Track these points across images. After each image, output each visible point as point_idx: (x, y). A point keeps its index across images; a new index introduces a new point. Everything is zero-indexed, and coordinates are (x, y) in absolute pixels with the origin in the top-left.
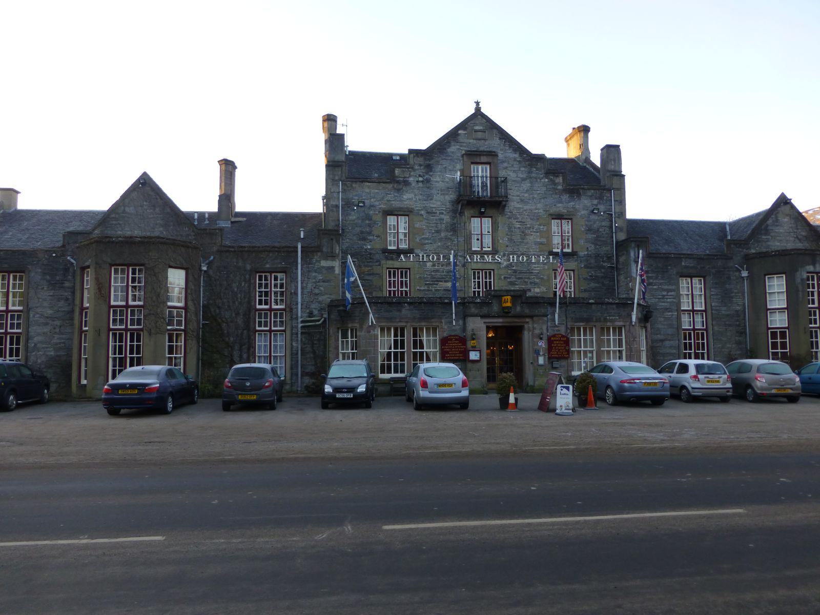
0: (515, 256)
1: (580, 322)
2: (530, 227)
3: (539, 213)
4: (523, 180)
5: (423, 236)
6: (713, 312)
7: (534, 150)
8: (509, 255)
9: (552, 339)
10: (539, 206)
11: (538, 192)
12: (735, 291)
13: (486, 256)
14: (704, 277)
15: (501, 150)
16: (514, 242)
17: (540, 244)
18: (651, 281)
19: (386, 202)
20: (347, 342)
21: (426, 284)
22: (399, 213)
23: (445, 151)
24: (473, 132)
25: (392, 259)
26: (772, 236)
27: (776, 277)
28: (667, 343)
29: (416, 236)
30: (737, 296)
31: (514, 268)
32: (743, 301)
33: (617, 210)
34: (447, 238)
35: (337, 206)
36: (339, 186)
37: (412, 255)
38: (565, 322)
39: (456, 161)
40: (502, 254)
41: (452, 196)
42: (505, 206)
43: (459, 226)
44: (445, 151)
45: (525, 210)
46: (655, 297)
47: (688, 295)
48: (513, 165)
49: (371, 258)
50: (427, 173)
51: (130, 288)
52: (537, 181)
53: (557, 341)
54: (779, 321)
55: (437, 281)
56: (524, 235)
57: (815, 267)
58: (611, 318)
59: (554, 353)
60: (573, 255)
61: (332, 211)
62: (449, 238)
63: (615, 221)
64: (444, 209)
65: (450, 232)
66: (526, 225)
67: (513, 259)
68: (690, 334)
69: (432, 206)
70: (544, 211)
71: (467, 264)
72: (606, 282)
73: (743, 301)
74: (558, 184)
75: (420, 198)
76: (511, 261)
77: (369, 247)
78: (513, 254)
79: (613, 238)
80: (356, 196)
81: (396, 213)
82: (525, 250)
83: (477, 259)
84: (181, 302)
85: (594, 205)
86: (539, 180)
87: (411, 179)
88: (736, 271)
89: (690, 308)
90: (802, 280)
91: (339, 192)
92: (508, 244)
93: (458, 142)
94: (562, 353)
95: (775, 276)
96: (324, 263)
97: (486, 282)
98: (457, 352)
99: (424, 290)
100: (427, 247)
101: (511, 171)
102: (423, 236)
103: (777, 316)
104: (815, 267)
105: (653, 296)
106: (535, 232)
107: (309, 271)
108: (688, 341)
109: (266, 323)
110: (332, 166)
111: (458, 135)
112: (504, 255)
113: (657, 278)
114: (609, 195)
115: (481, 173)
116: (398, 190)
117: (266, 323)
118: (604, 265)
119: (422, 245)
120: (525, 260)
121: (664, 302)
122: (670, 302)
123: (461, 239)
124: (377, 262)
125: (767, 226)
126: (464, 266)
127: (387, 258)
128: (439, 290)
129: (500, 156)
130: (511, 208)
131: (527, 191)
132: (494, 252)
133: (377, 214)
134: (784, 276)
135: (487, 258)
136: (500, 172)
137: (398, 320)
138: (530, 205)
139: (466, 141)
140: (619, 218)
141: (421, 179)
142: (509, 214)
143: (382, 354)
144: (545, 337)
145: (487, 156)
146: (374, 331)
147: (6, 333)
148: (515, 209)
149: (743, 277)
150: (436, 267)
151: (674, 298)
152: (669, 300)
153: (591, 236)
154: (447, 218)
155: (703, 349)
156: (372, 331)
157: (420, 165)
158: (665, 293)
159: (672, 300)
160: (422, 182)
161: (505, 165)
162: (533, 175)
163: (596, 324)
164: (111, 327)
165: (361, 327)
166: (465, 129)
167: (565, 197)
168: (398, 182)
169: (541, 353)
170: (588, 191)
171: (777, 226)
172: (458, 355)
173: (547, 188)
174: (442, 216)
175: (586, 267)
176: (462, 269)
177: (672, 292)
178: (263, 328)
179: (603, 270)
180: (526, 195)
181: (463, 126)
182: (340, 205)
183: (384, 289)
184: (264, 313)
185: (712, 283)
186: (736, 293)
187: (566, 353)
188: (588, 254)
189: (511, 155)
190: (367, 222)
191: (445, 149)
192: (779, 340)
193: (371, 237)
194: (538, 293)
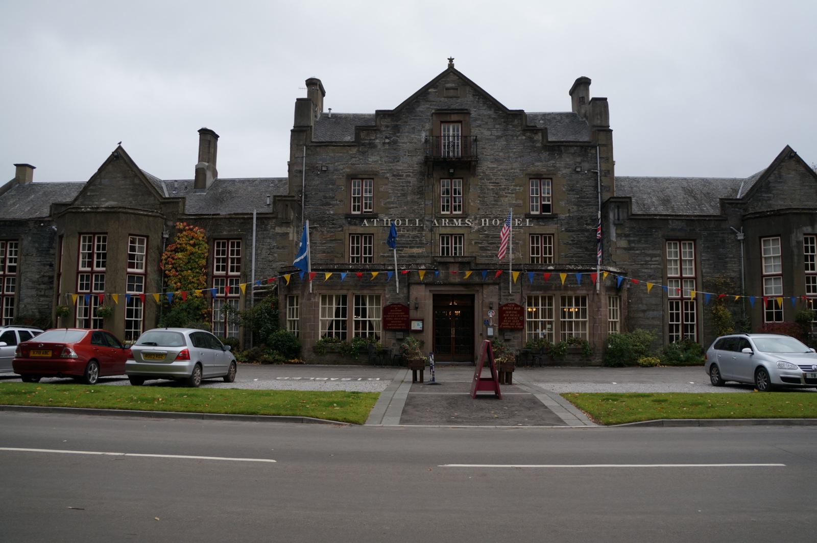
0: (487, 220)
1: (537, 291)
2: (505, 188)
3: (514, 173)
4: (498, 137)
5: (388, 200)
7: (511, 104)
8: (481, 218)
9: (504, 308)
10: (515, 165)
11: (514, 150)
12: (730, 256)
13: (455, 220)
14: (695, 241)
15: (475, 107)
16: (487, 205)
17: (516, 206)
18: (633, 245)
19: (350, 165)
20: (293, 309)
22: (364, 176)
23: (414, 111)
24: (445, 90)
25: (355, 224)
27: (772, 240)
28: (650, 314)
29: (381, 200)
31: (486, 233)
32: (736, 268)
33: (603, 169)
34: (413, 202)
35: (301, 172)
36: (303, 151)
37: (375, 220)
39: (425, 120)
40: (473, 217)
41: (420, 158)
42: (475, 167)
43: (427, 188)
44: (414, 111)
45: (499, 170)
46: (637, 263)
47: (677, 260)
48: (487, 123)
49: (333, 224)
50: (394, 134)
51: (95, 256)
53: (509, 310)
54: (774, 290)
55: (402, 247)
56: (498, 196)
57: (813, 228)
58: (572, 286)
59: (506, 324)
60: (553, 218)
61: (296, 176)
62: (415, 202)
63: (600, 180)
64: (411, 171)
66: (501, 186)
67: (485, 222)
68: (677, 304)
69: (399, 168)
70: (521, 170)
71: (435, 228)
73: (736, 268)
74: (537, 141)
75: (386, 161)
76: (483, 225)
77: (332, 212)
78: (485, 217)
79: (598, 198)
81: (360, 176)
82: (498, 213)
83: (445, 224)
84: (142, 269)
85: (577, 162)
86: (515, 138)
87: (378, 141)
89: (678, 275)
90: (799, 243)
91: (303, 157)
92: (480, 206)
93: (427, 101)
94: (515, 323)
95: (771, 238)
96: (278, 230)
97: (545, 248)
98: (399, 322)
100: (392, 211)
101: (485, 129)
102: (388, 200)
103: (773, 283)
104: (813, 228)
105: (635, 262)
106: (509, 193)
107: (264, 238)
109: (222, 289)
110: (299, 133)
111: (429, 93)
112: (476, 218)
113: (639, 242)
114: (594, 152)
115: (451, 132)
116: (363, 153)
117: (222, 289)
118: (588, 228)
119: (386, 210)
120: (498, 224)
121: (647, 268)
123: (429, 203)
124: (340, 227)
125: (769, 182)
126: (431, 230)
127: (350, 223)
128: (403, 257)
129: (473, 114)
130: (485, 168)
131: (502, 150)
132: (464, 216)
133: (340, 178)
134: (779, 238)
135: (456, 222)
136: (472, 131)
137: (339, 288)
138: (506, 164)
140: (605, 176)
141: (387, 141)
142: (482, 174)
143: (323, 322)
144: (496, 307)
145: (461, 115)
146: (315, 299)
147: (3, 295)
148: (488, 169)
150: (402, 232)
151: (658, 264)
152: (652, 266)
154: (413, 180)
155: (692, 320)
156: (312, 299)
157: (387, 127)
158: (648, 259)
159: (656, 266)
160: (388, 143)
161: (479, 122)
162: (510, 133)
163: (555, 292)
165: (303, 295)
166: (435, 88)
167: (545, 155)
168: (363, 145)
169: (491, 324)
172: (400, 325)
173: (524, 146)
175: (567, 230)
176: (429, 235)
177: (656, 257)
179: (586, 234)
180: (501, 154)
181: (433, 84)
182: (304, 170)
183: (346, 257)
184: (12, 279)
185: (704, 247)
186: (731, 258)
187: (520, 324)
188: (569, 216)
189: (486, 112)
190: (331, 186)
191: (414, 109)
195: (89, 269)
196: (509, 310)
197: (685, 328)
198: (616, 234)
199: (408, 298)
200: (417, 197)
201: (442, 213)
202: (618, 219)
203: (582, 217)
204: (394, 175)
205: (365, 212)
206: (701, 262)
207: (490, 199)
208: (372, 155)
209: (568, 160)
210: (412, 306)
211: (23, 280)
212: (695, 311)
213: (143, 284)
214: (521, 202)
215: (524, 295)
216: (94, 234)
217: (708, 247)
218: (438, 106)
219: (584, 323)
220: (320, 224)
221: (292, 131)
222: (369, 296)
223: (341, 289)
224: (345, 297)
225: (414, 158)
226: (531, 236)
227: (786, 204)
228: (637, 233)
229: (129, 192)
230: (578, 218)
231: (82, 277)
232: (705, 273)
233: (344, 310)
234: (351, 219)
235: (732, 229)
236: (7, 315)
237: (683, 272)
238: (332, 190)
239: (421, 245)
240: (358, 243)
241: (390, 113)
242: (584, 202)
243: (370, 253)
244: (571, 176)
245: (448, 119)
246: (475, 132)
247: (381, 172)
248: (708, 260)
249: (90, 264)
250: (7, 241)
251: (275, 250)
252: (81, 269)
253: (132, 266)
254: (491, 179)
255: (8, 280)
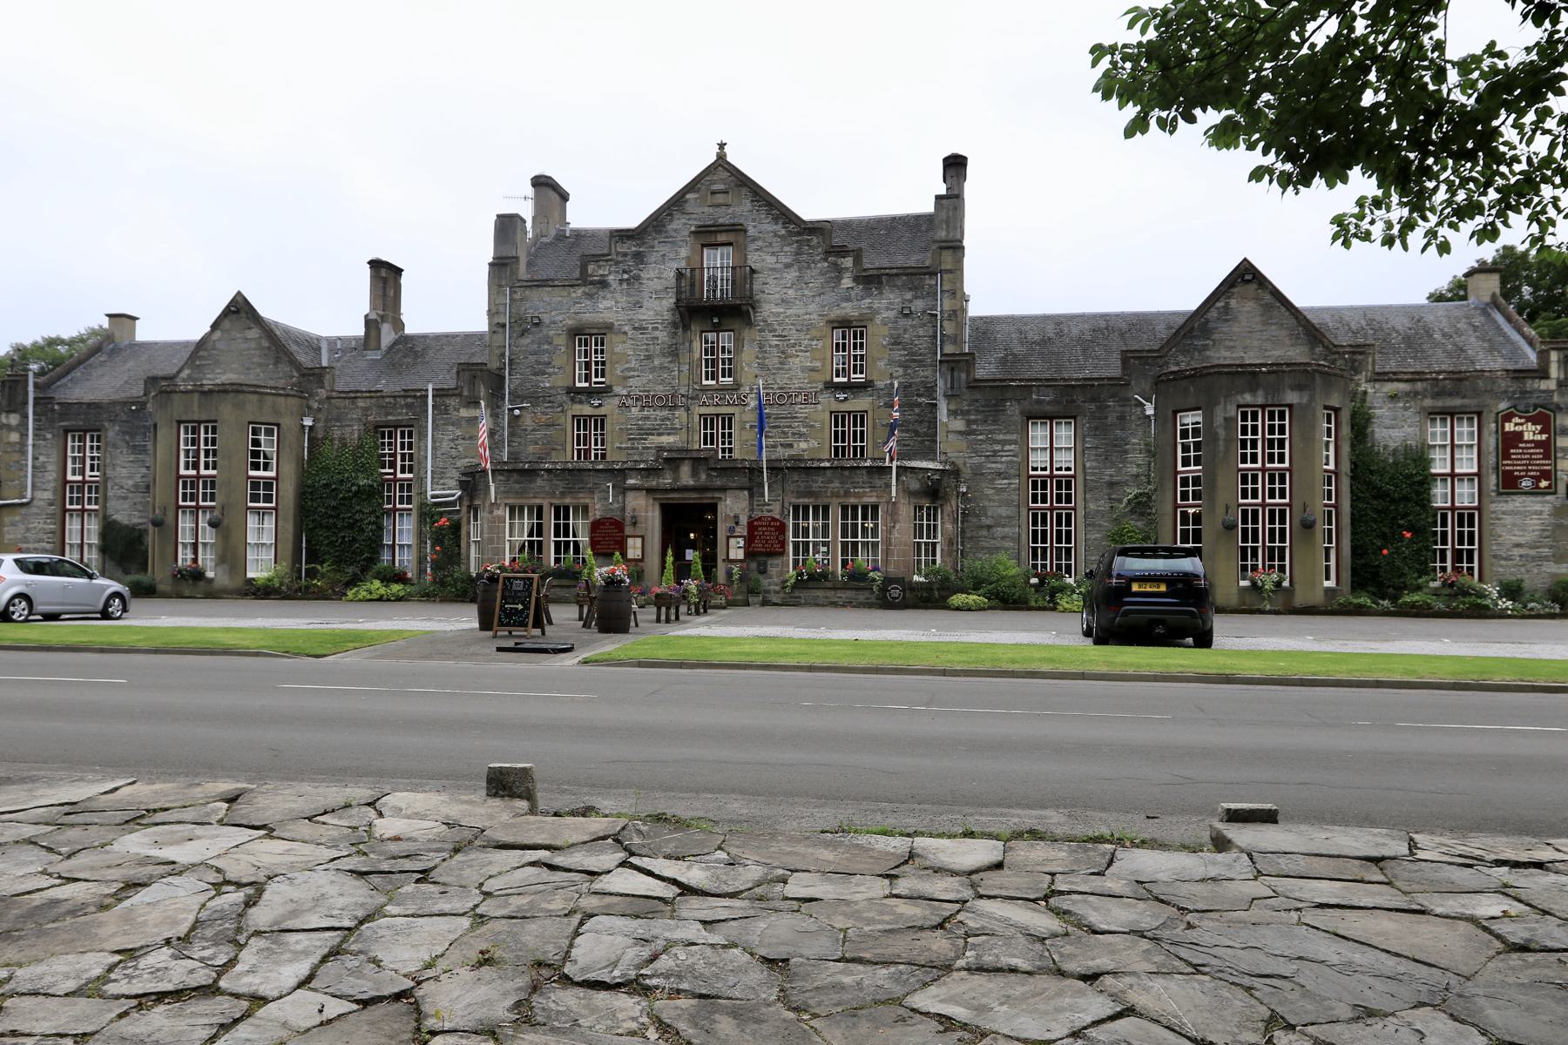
3: (810, 320)
4: (788, 266)
6: (1088, 478)
7: (809, 209)
9: (756, 523)
10: (812, 308)
12: (1134, 441)
15: (754, 220)
16: (769, 370)
18: (975, 427)
21: (629, 439)
25: (581, 402)
26: (1213, 340)
28: (999, 531)
30: (1134, 450)
34: (662, 368)
38: (780, 498)
41: (670, 301)
45: (787, 317)
48: (771, 244)
49: (550, 402)
51: (202, 454)
52: (809, 268)
53: (762, 526)
55: (647, 434)
56: (785, 356)
65: (667, 357)
69: (641, 317)
72: (923, 429)
77: (547, 385)
80: (531, 308)
81: (587, 331)
82: (785, 381)
87: (611, 277)
88: (1136, 406)
89: (1448, 470)
90: (1229, 421)
93: (683, 213)
96: (464, 413)
99: (627, 448)
105: (975, 452)
106: (802, 351)
108: (1466, 529)
115: (717, 261)
116: (590, 296)
117: (1255, 491)
121: (996, 462)
122: (1007, 462)
125: (1208, 321)
128: (648, 448)
129: (751, 231)
139: (700, 210)
141: (626, 276)
149: (1149, 416)
151: (1014, 456)
152: (1004, 459)
153: (899, 354)
154: (663, 336)
155: (1471, 542)
158: (998, 447)
161: (760, 243)
164: (181, 503)
170: (896, 278)
171: (1227, 320)
174: (657, 333)
178: (188, 503)
179: (917, 410)
180: (790, 292)
181: (692, 186)
186: (1134, 444)
189: (768, 226)
190: (546, 347)
192: (1039, 528)
193: (551, 370)
194: (803, 451)
195: (194, 472)
196: (762, 526)
197: (1458, 556)
198: (948, 410)
199: (623, 509)
200: (667, 360)
201: (704, 382)
202: (952, 388)
203: (910, 385)
204: (635, 329)
205: (595, 383)
206: (1083, 451)
207: (773, 361)
208: (604, 298)
209: (891, 296)
210: (628, 521)
211: (109, 487)
212: (1476, 529)
213: (274, 493)
214: (818, 364)
215: (786, 505)
216: (199, 422)
217: (1096, 428)
218: (699, 220)
219: (875, 545)
220: (531, 403)
221: (490, 264)
222: (814, 507)
223: (534, 497)
224: (540, 509)
225: (664, 302)
226: (1240, 410)
227: (1235, 355)
228: (981, 409)
229: (255, 360)
230: (905, 387)
231: (185, 483)
232: (1090, 468)
233: (540, 526)
234: (573, 393)
235: (1136, 399)
236: (557, 534)
237: (1457, 464)
238: (547, 351)
239: (673, 431)
240: (585, 429)
241: (630, 233)
242: (915, 361)
243: (862, 441)
244: (896, 322)
245: (712, 240)
246: (754, 259)
247: (616, 324)
248: (1096, 448)
249: (196, 466)
250: (86, 431)
251: (460, 442)
252: (183, 472)
253: (256, 466)
254: (775, 330)
255: (90, 488)
